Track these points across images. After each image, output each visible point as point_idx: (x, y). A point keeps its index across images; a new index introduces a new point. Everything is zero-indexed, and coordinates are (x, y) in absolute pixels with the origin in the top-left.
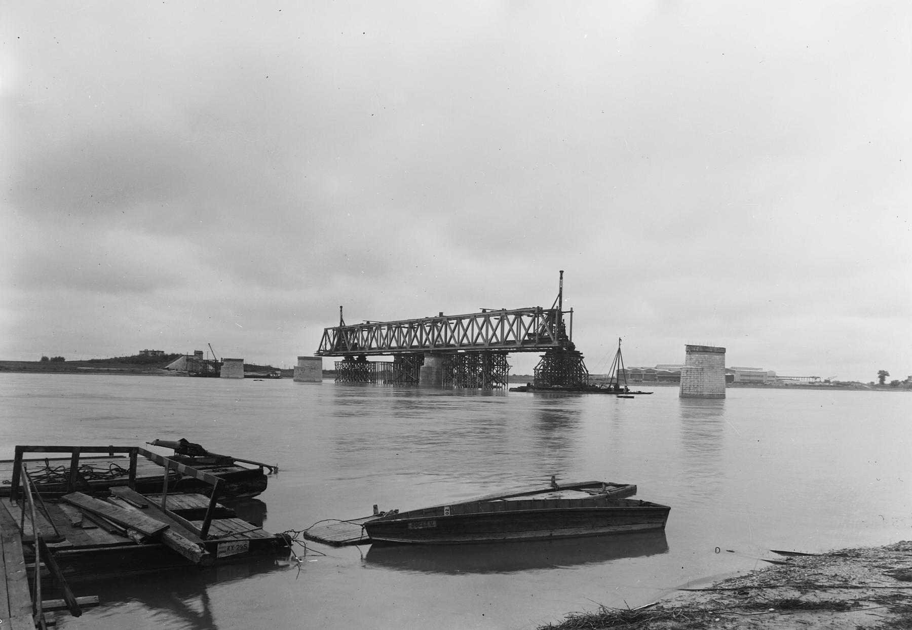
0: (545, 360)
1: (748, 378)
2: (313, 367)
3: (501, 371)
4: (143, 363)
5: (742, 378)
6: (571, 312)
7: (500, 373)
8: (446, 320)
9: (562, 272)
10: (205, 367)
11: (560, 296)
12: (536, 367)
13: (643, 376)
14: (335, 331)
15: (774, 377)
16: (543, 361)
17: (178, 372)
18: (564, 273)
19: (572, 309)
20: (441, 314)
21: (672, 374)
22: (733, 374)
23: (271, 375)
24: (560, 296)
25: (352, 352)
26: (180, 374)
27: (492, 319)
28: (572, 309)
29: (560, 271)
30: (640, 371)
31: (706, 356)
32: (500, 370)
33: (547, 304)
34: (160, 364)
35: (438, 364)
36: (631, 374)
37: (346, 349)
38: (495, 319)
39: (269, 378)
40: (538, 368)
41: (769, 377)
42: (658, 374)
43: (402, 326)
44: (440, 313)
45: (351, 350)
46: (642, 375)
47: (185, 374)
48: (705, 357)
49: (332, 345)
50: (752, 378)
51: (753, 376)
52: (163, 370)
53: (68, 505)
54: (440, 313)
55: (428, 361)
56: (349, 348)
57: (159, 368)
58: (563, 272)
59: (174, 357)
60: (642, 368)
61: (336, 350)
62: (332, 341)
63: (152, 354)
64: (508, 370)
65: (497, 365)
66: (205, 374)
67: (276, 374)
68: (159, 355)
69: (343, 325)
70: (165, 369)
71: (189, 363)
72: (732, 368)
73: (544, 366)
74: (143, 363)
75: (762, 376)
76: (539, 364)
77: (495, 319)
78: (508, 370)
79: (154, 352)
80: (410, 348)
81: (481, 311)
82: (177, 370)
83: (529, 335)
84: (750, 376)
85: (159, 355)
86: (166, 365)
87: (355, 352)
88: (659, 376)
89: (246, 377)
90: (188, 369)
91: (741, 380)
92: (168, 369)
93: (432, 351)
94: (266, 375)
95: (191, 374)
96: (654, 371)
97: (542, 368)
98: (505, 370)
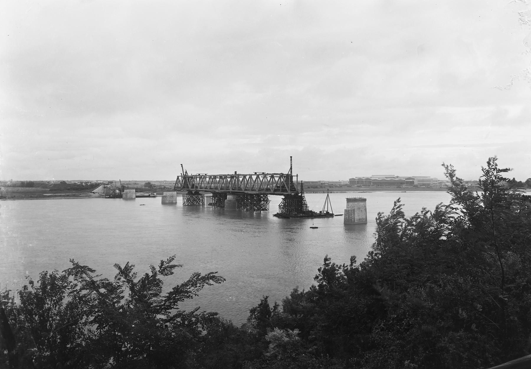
0: (284, 201)
1: (422, 182)
2: (172, 195)
3: (265, 203)
4: (79, 190)
5: (419, 182)
6: (297, 176)
7: (265, 204)
8: (237, 176)
9: (291, 157)
10: (114, 190)
11: (291, 168)
12: (279, 205)
13: (364, 182)
14: (183, 178)
15: (437, 181)
16: (283, 201)
17: (99, 195)
18: (292, 158)
19: (297, 174)
20: (236, 172)
21: (381, 181)
22: (414, 180)
23: (151, 195)
24: (291, 168)
25: (192, 189)
26: (100, 196)
27: (260, 176)
28: (297, 174)
29: (290, 157)
30: (362, 179)
31: (356, 203)
32: (265, 203)
33: (286, 172)
34: (89, 190)
35: (234, 198)
36: (357, 181)
37: (188, 187)
38: (262, 177)
39: (150, 197)
40: (281, 205)
41: (434, 181)
42: (372, 181)
43: (217, 177)
44: (235, 172)
45: (191, 188)
46: (363, 181)
47: (103, 195)
48: (355, 204)
49: (181, 185)
50: (424, 182)
51: (425, 181)
52: (91, 194)
53: (15, 184)
54: (235, 172)
55: (229, 197)
56: (190, 187)
57: (88, 192)
58: (292, 157)
59: (97, 185)
60: (363, 177)
61: (184, 187)
62: (181, 183)
63: (85, 184)
64: (269, 202)
65: (263, 200)
66: (115, 196)
67: (153, 194)
68: (89, 184)
69: (187, 175)
70: (92, 193)
71: (105, 189)
72: (413, 177)
73: (284, 204)
74: (79, 190)
75: (430, 181)
76: (281, 203)
77: (262, 177)
78: (269, 202)
79: (86, 183)
80: (220, 189)
81: (254, 173)
82: (99, 193)
83: (277, 187)
84: (423, 181)
85: (89, 184)
86: (93, 191)
87: (193, 189)
88: (373, 182)
89: (137, 197)
90: (105, 192)
91: (418, 184)
92: (93, 193)
93: (231, 192)
94: (148, 195)
95: (106, 196)
96: (370, 179)
97: (283, 205)
98: (267, 203)
